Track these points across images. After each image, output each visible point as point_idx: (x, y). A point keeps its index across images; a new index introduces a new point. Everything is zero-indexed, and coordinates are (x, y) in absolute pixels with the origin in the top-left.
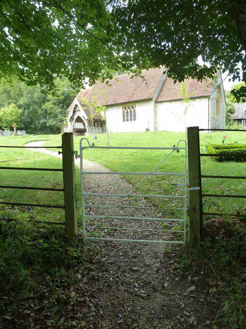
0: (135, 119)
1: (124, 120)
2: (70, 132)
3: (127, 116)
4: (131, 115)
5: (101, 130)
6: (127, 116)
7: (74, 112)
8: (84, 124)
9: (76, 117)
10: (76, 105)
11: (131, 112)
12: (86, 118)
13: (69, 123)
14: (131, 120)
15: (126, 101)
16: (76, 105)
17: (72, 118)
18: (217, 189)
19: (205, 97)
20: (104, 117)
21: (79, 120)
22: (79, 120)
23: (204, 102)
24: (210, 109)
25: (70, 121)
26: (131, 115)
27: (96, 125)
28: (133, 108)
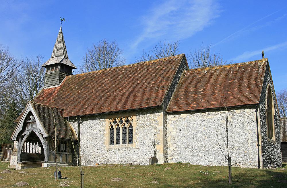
0: (131, 141)
1: (112, 143)
2: (189, 64)
3: (118, 135)
4: (124, 134)
5: (70, 158)
6: (118, 135)
7: (25, 125)
8: (41, 146)
9: (27, 133)
10: (30, 113)
11: (124, 128)
12: (45, 135)
13: (16, 142)
14: (124, 142)
15: (116, 110)
16: (30, 113)
17: (20, 136)
18: (272, 164)
19: (250, 107)
20: (77, 135)
21: (33, 138)
22: (33, 138)
23: (250, 113)
24: (259, 126)
25: (18, 139)
26: (124, 134)
27: (63, 149)
28: (127, 121)
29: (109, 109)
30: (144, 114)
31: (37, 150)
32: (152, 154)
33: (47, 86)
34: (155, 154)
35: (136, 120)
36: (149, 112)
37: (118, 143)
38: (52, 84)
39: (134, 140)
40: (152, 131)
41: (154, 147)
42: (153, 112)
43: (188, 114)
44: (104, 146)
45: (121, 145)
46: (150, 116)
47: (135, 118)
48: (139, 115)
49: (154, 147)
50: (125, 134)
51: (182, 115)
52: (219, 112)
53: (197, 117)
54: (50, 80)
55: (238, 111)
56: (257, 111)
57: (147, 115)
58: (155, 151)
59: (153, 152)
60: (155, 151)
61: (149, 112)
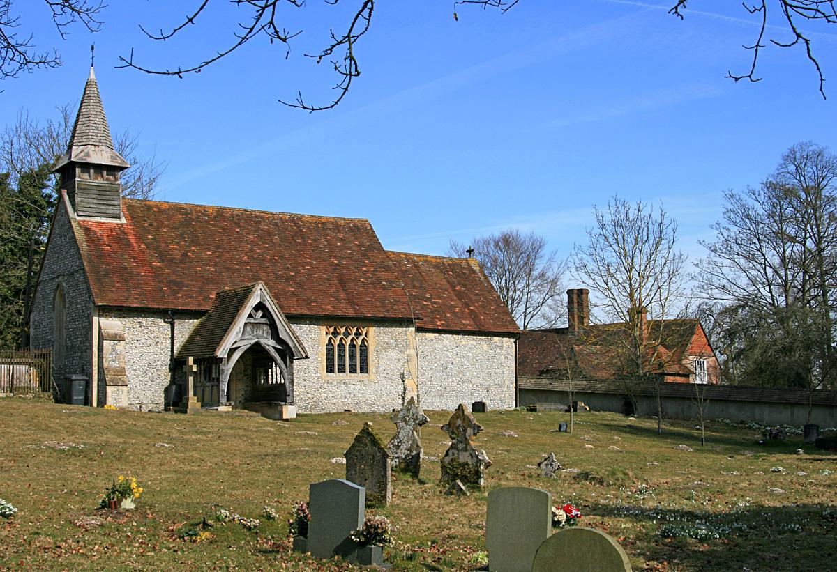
0: (364, 369)
1: (330, 369)
3: (341, 357)
26: (352, 356)
29: (329, 310)
30: (387, 327)
31: (279, 379)
32: (400, 393)
33: (87, 214)
34: (404, 393)
35: (374, 335)
36: (99, 312)
37: (341, 370)
38: (99, 211)
39: (372, 368)
40: (399, 356)
41: (403, 381)
42: (401, 326)
43: (436, 335)
44: (319, 375)
45: (346, 376)
46: (397, 331)
47: (373, 331)
48: (392, 327)
49: (403, 381)
50: (339, 355)
51: (428, 335)
52: (475, 337)
53: (448, 339)
54: (95, 201)
55: (496, 339)
56: (515, 342)
57: (393, 329)
58: (405, 389)
59: (401, 391)
60: (405, 389)
61: (99, 312)
